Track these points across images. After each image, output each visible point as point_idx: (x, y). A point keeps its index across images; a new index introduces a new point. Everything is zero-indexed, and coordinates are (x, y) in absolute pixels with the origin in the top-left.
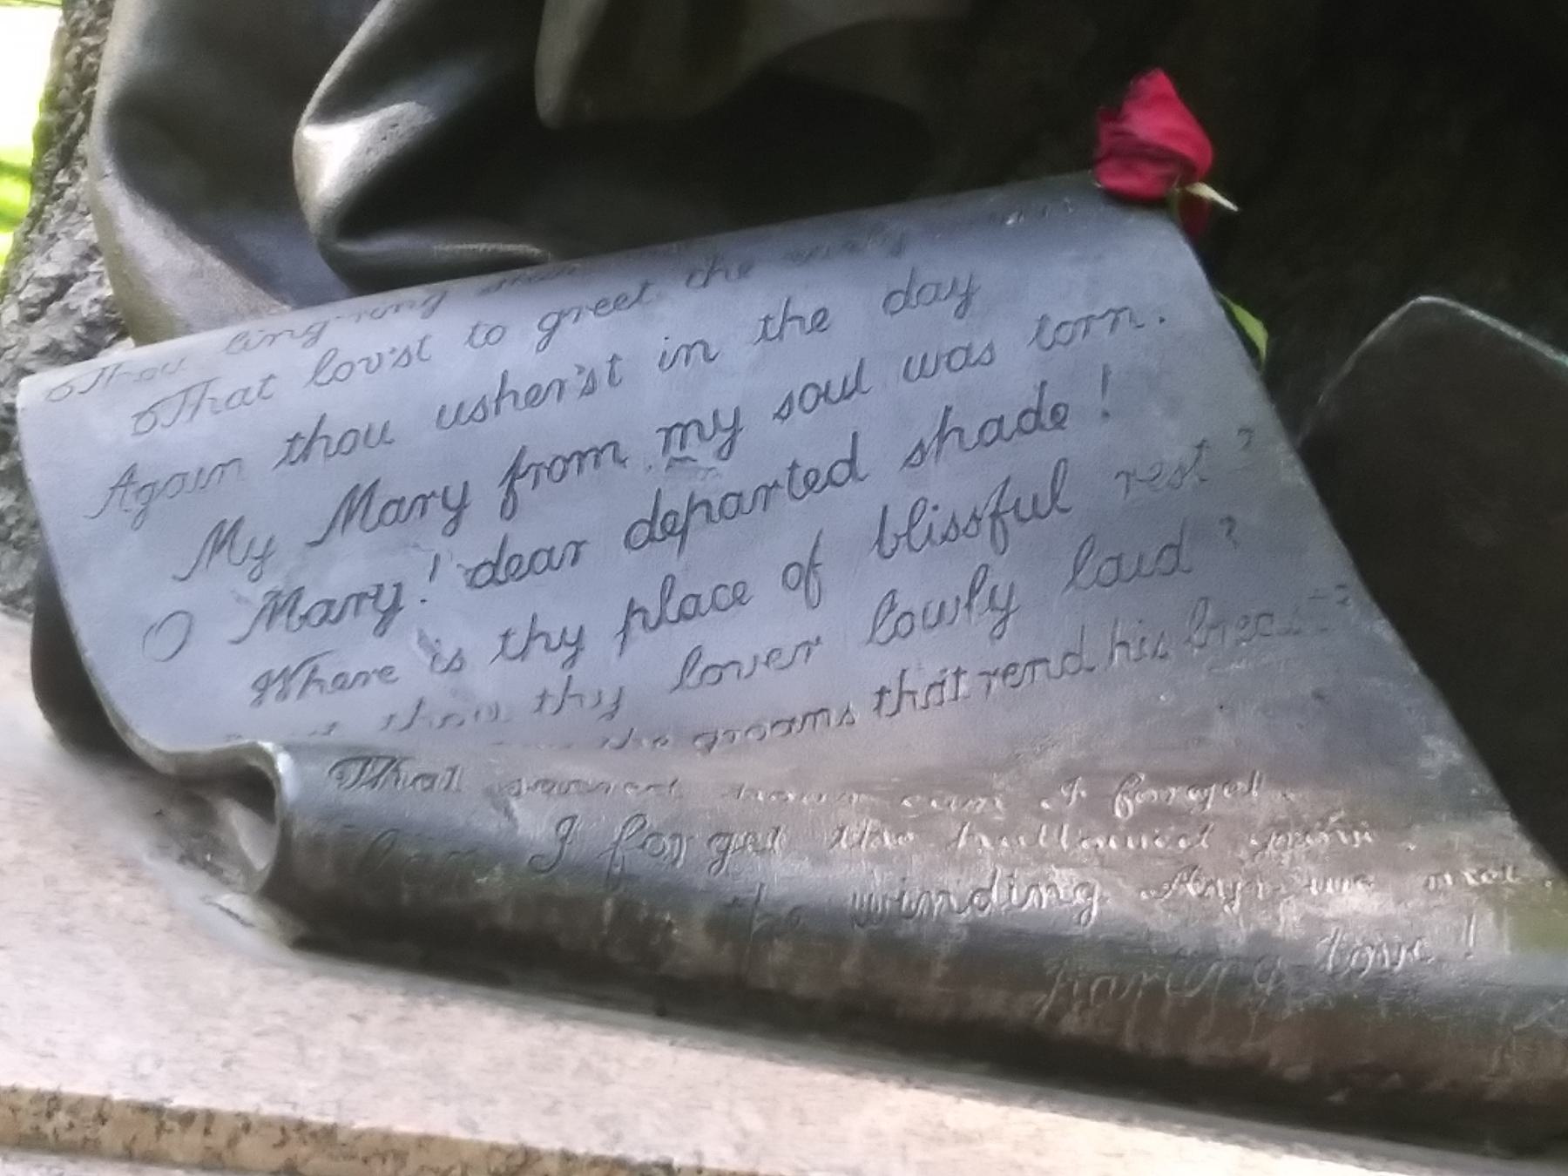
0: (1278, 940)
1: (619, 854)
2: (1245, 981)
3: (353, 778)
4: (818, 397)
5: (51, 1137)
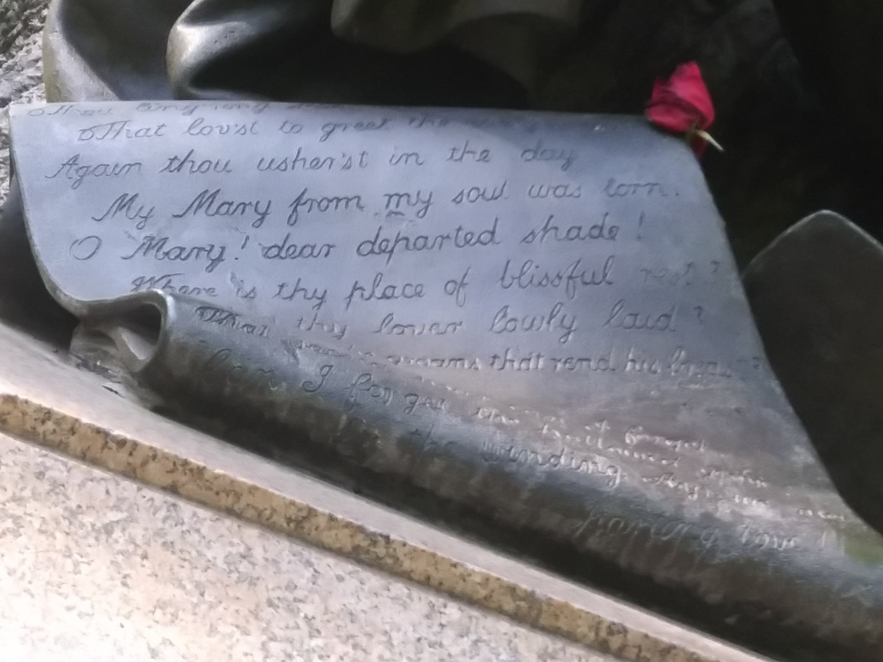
0: (718, 520)
1: (354, 391)
2: (696, 538)
3: (209, 316)
4: (479, 196)
5: (41, 436)
